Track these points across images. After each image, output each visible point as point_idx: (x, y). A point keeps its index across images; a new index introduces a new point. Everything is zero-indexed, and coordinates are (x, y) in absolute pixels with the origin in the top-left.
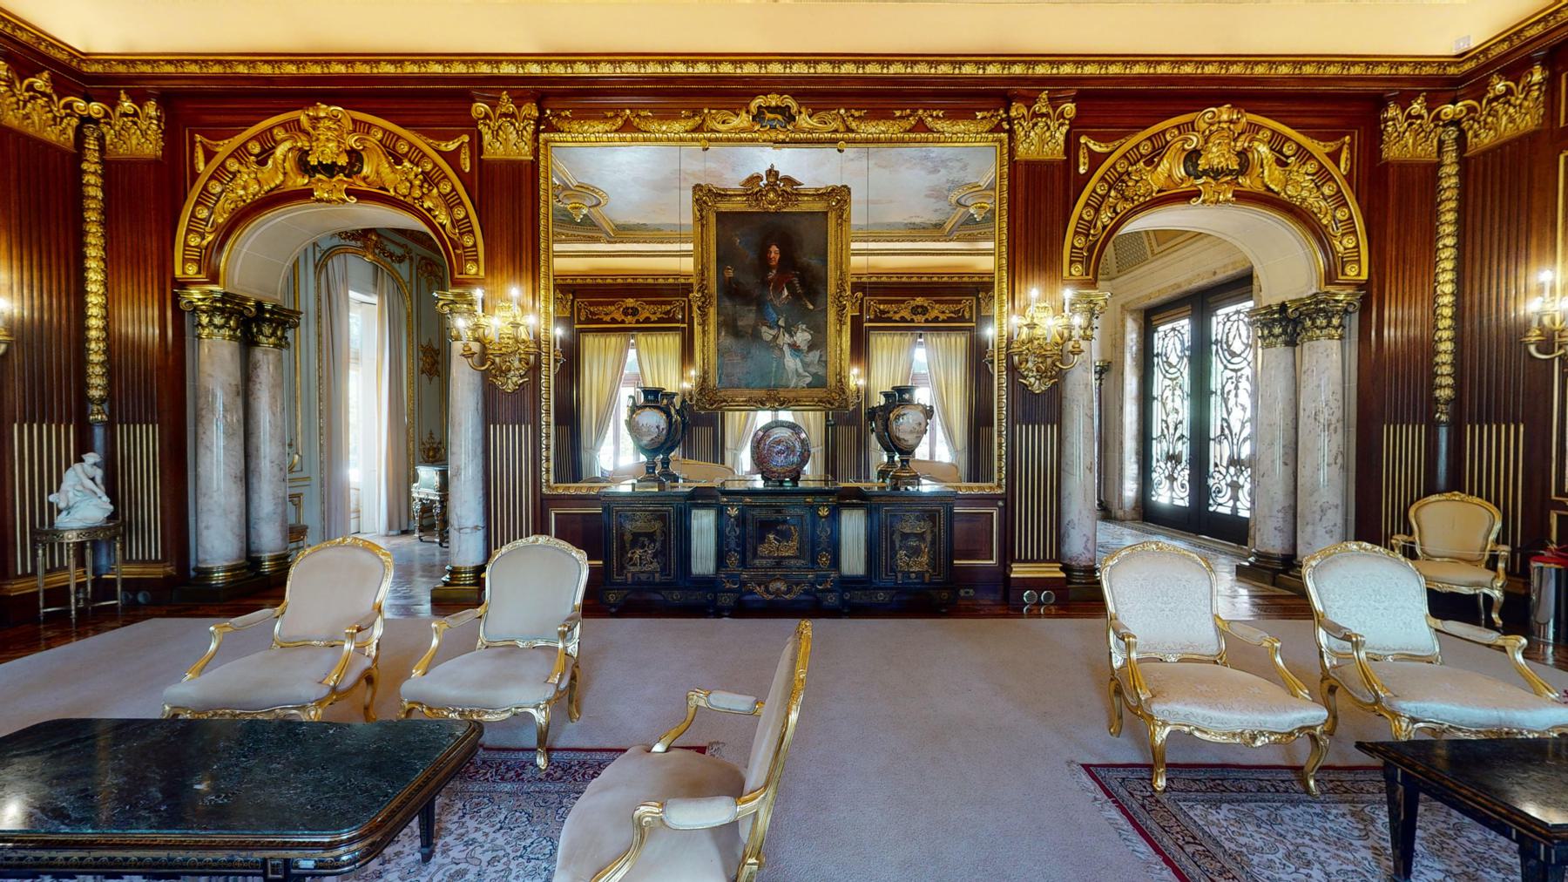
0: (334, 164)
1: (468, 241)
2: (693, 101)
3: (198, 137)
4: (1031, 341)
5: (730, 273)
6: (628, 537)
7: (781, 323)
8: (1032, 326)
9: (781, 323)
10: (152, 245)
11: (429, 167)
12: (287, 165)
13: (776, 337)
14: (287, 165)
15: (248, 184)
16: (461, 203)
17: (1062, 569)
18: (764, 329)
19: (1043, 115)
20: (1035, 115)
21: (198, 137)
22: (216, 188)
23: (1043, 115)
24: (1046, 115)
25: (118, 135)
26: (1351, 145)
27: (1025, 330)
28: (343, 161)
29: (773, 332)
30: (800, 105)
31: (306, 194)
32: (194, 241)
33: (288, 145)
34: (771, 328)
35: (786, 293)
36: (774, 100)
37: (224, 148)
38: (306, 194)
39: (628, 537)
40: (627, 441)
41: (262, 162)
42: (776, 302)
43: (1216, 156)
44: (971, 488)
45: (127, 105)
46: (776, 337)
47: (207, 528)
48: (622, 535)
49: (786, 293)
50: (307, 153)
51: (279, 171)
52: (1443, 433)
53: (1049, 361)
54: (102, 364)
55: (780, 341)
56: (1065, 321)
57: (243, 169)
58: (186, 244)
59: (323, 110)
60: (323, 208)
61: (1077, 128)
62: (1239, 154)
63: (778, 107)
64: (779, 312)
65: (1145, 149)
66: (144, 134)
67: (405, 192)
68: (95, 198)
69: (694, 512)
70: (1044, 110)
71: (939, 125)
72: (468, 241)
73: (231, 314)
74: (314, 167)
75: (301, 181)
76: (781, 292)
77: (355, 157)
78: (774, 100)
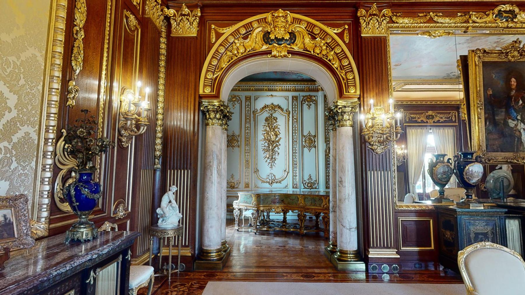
0: (283, 38)
1: (350, 76)
2: (466, 9)
3: (213, 26)
4: (372, 126)
5: (490, 92)
6: (472, 236)
7: (519, 118)
8: (373, 119)
9: (519, 118)
10: (192, 79)
11: (329, 41)
12: (257, 40)
13: (516, 125)
14: (257, 40)
15: (241, 47)
16: (347, 57)
17: (398, 253)
18: (510, 121)
19: (374, 15)
20: (370, 15)
21: (213, 26)
22: (222, 50)
23: (374, 15)
24: (188, 15)
25: (178, 24)
26: (349, 29)
27: (370, 121)
28: (287, 37)
29: (515, 122)
30: (520, 10)
31: (268, 53)
32: (210, 76)
33: (260, 29)
34: (513, 120)
35: (521, 102)
36: (508, 7)
37: (228, 31)
38: (268, 53)
39: (472, 236)
40: (429, 180)
41: (245, 38)
42: (516, 107)
43: (280, 33)
44: (415, 206)
45: (186, 11)
46: (516, 125)
47: (211, 227)
48: (469, 234)
49: (521, 102)
50: (269, 33)
51: (255, 41)
52: (158, 173)
53: (385, 136)
54: (161, 138)
55: (519, 127)
56: (390, 116)
57: (236, 41)
58: (206, 78)
59: (281, 12)
60: (274, 60)
61: (202, 23)
62: (290, 33)
63: (510, 10)
64: (517, 112)
65: (243, 31)
66: (191, 24)
67: (318, 52)
68: (164, 55)
69: (507, 221)
70: (374, 12)
71: (440, 20)
72: (350, 76)
73: (217, 112)
74: (272, 40)
75: (265, 47)
76: (518, 102)
77: (293, 36)
78: (508, 7)
